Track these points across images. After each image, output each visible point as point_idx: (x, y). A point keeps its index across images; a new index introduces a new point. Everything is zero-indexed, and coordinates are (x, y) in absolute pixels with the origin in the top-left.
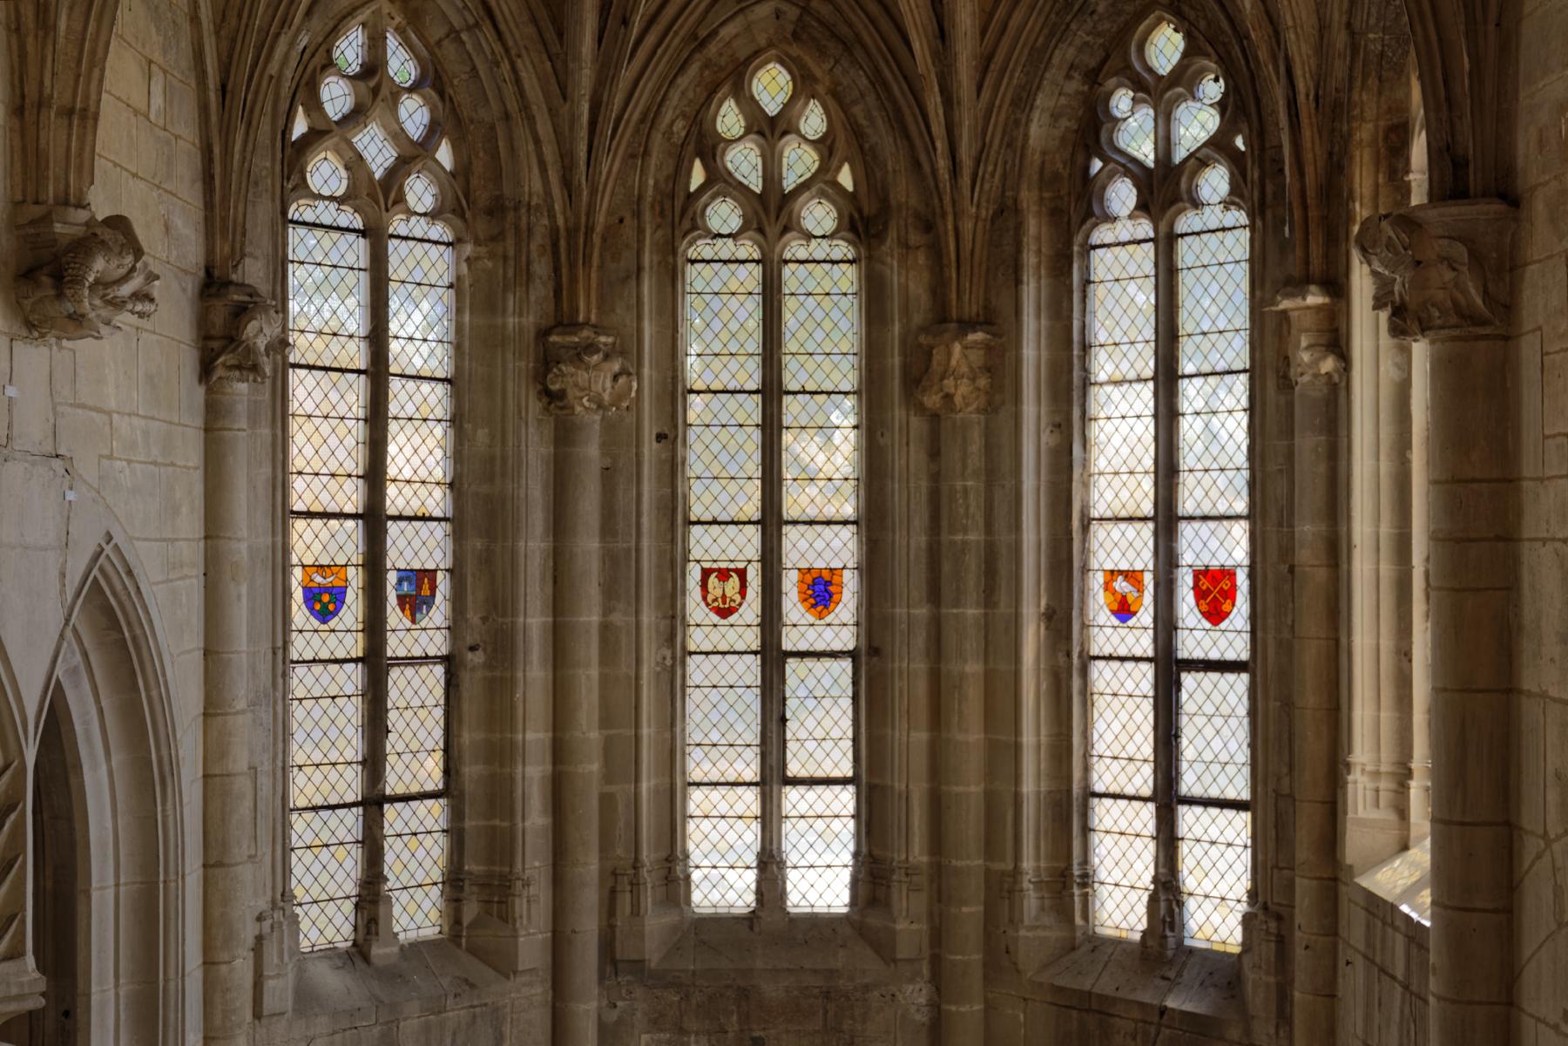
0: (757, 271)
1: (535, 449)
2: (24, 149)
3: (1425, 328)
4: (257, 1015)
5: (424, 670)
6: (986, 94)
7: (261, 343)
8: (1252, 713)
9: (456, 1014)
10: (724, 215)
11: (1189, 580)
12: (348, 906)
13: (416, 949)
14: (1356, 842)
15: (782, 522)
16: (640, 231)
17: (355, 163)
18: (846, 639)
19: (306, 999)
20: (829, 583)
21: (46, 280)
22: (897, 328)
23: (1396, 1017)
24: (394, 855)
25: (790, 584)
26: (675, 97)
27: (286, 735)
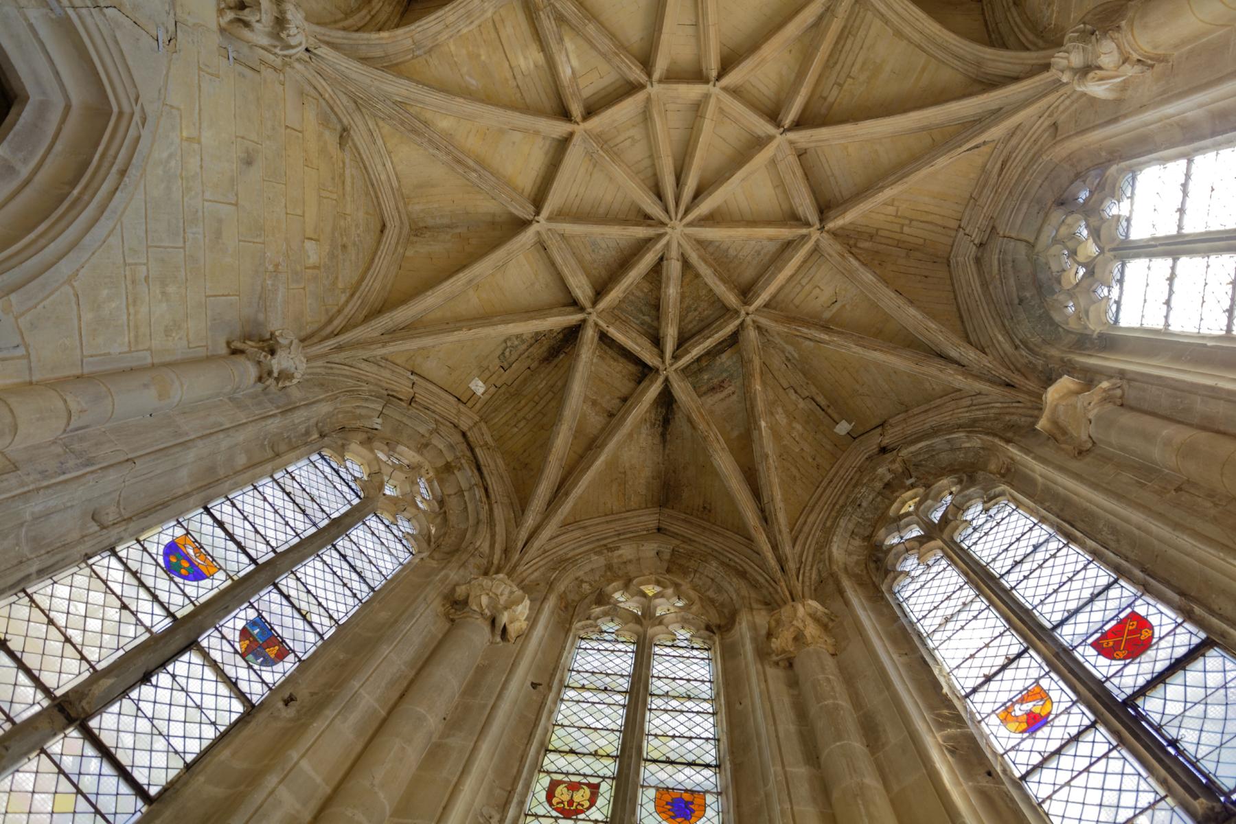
11: (1091, 651)
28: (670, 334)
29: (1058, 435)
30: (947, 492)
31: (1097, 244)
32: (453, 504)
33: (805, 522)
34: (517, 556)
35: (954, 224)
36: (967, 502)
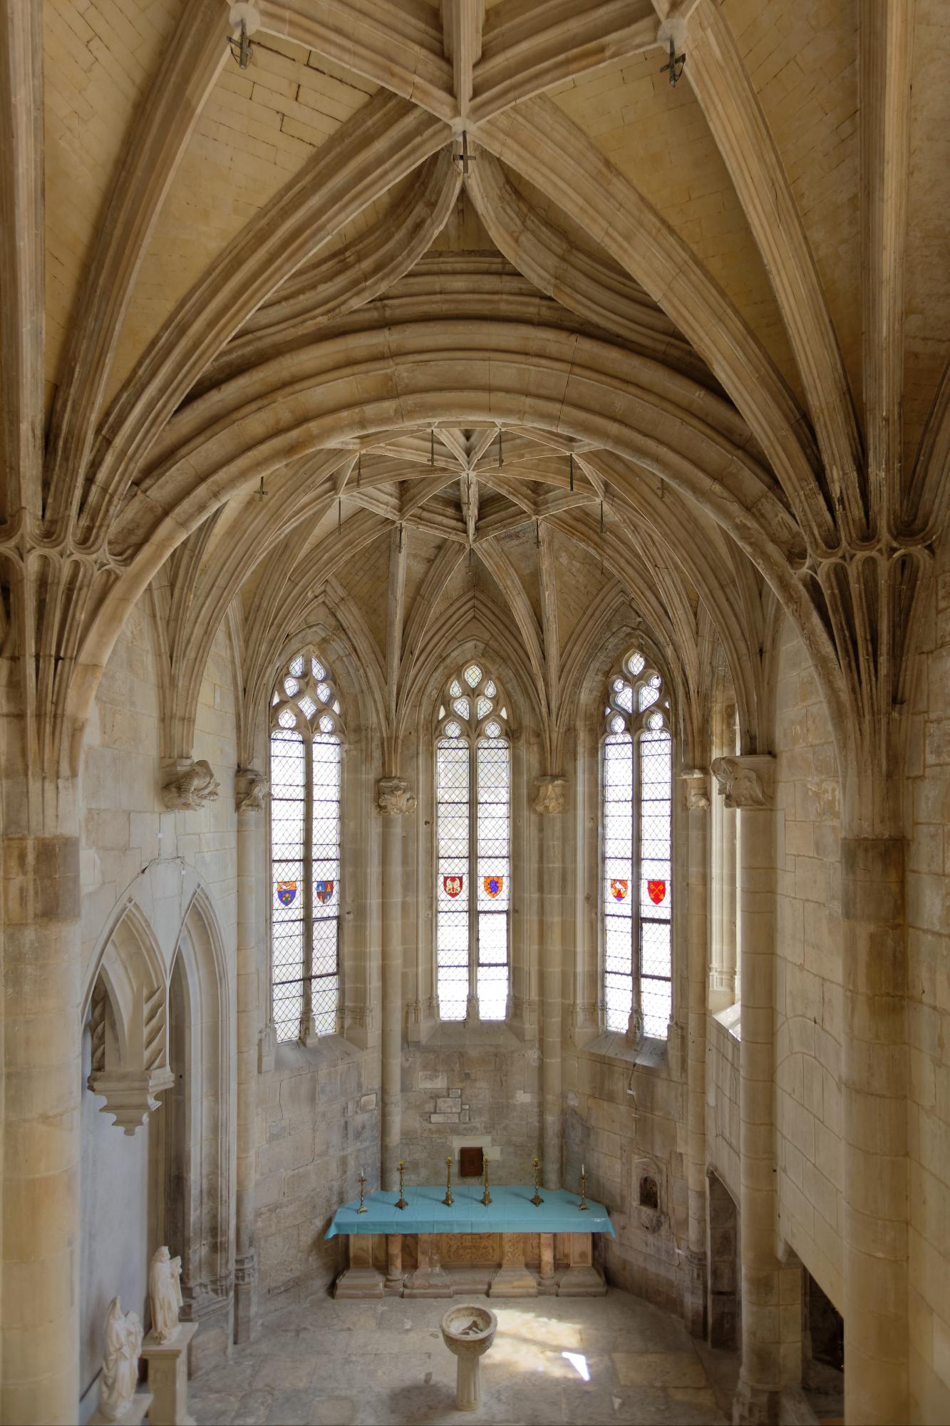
0: (467, 752)
1: (374, 829)
2: (165, 735)
3: (739, 805)
4: (260, 1072)
5: (328, 922)
6: (562, 681)
7: (261, 795)
8: (672, 941)
9: (342, 1067)
10: (453, 729)
12: (297, 1022)
13: (325, 1040)
14: (712, 1001)
15: (477, 857)
16: (418, 737)
17: (299, 714)
18: (504, 906)
19: (280, 1064)
20: (497, 883)
21: (174, 789)
22: (525, 777)
23: (728, 1075)
24: (316, 999)
25: (481, 883)
26: (432, 682)
27: (271, 952)
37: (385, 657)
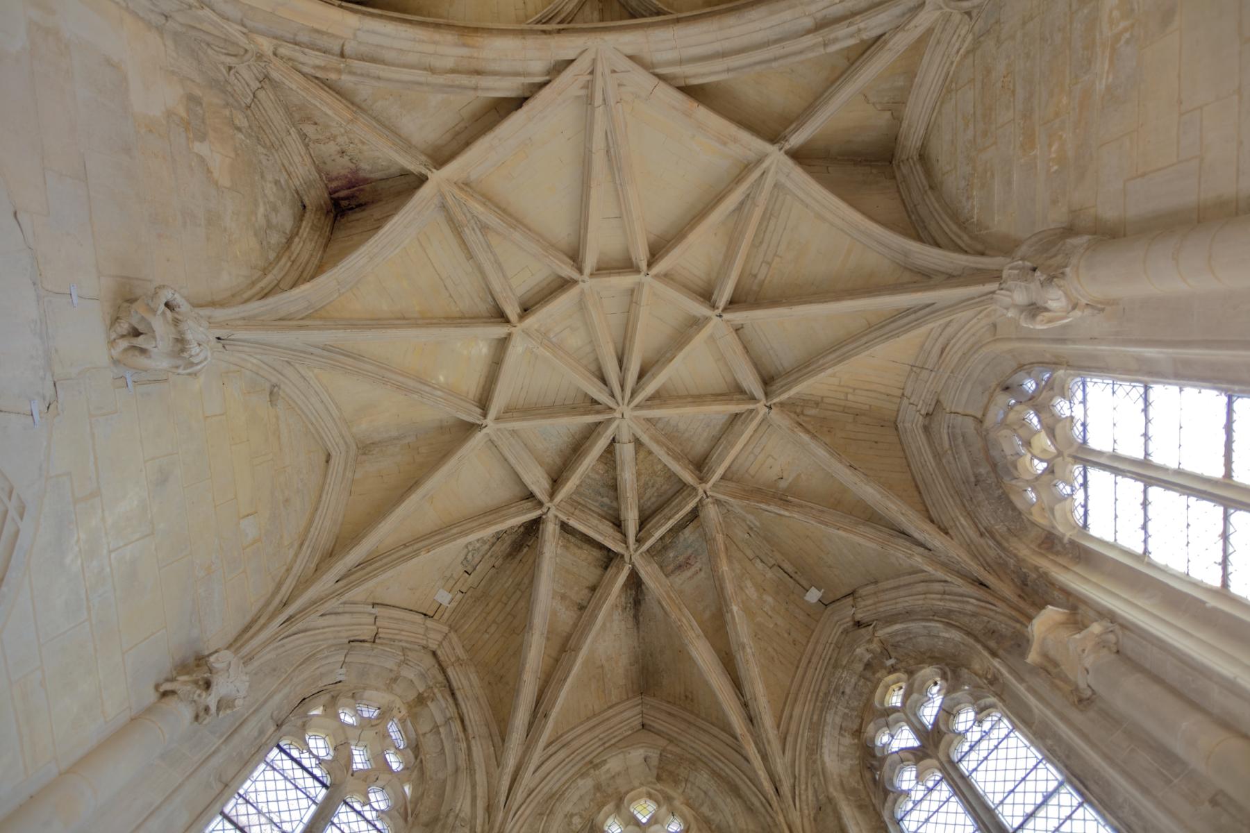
6: (788, 753)
28: (631, 518)
29: (1049, 669)
30: (931, 682)
31: (1054, 446)
32: (429, 744)
33: (791, 717)
34: (501, 815)
35: (899, 393)
36: (955, 706)
37: (503, 740)
